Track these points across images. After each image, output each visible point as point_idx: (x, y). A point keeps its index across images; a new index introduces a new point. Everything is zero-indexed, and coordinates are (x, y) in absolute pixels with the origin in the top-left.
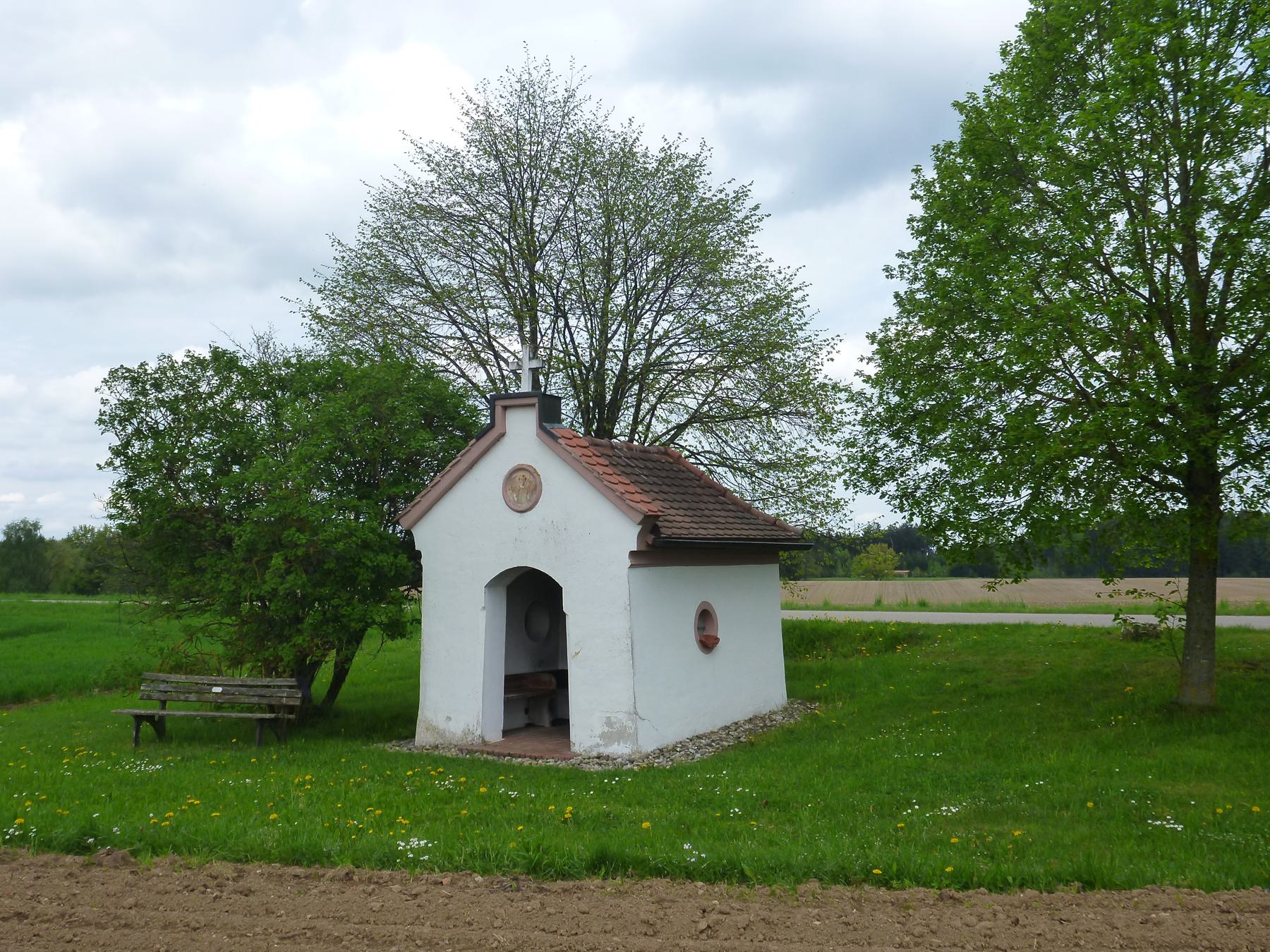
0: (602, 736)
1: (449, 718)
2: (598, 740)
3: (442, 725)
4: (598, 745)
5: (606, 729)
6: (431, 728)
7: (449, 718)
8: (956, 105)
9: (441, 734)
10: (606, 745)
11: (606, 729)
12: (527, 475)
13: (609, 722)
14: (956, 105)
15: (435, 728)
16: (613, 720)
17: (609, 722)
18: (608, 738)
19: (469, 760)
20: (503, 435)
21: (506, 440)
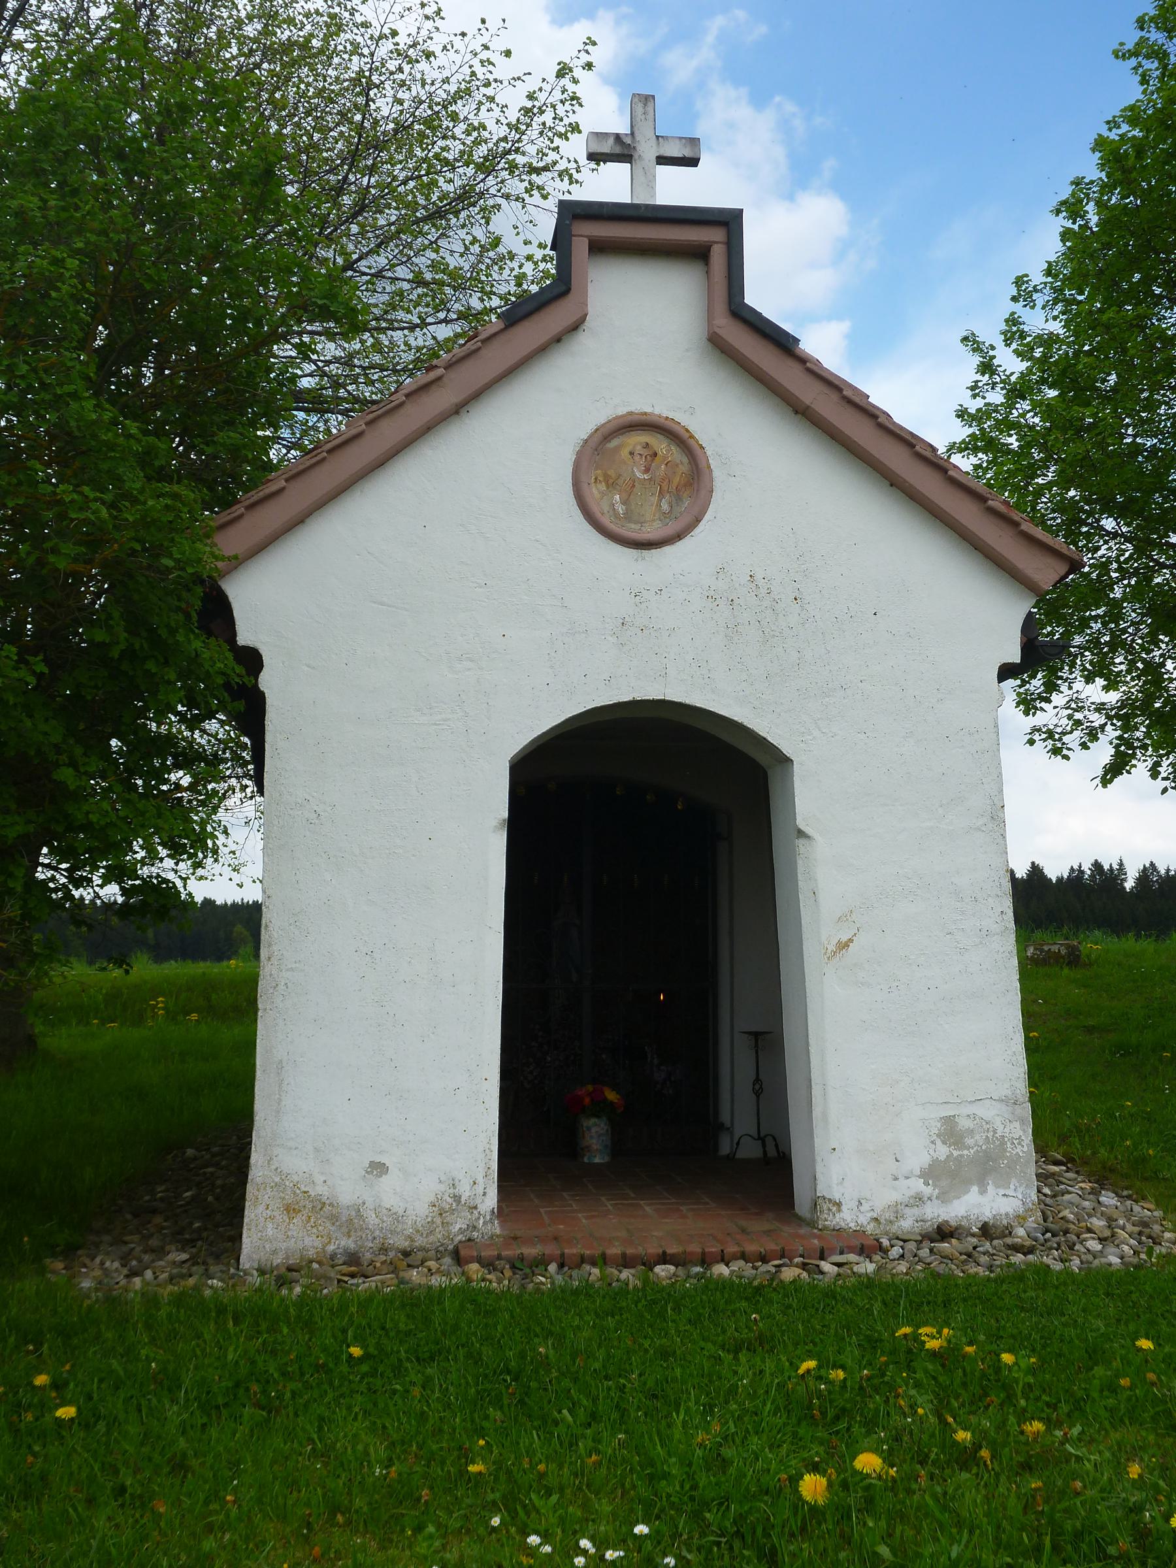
0: (930, 1173)
1: (378, 1169)
2: (918, 1185)
3: (346, 1187)
4: (919, 1199)
5: (942, 1151)
6: (300, 1205)
7: (378, 1169)
8: (1033, 863)
9: (351, 1221)
10: (944, 1197)
11: (942, 1151)
12: (661, 445)
13: (950, 1132)
14: (1033, 863)
15: (319, 1205)
16: (964, 1124)
17: (950, 1132)
18: (945, 1176)
19: (383, 1322)
20: (576, 327)
21: (584, 341)
